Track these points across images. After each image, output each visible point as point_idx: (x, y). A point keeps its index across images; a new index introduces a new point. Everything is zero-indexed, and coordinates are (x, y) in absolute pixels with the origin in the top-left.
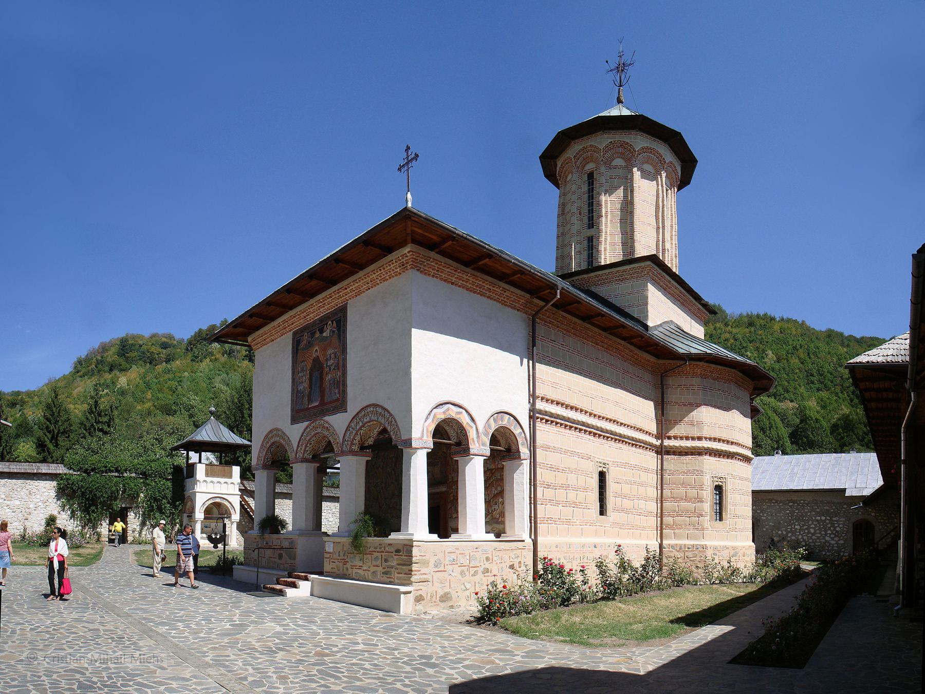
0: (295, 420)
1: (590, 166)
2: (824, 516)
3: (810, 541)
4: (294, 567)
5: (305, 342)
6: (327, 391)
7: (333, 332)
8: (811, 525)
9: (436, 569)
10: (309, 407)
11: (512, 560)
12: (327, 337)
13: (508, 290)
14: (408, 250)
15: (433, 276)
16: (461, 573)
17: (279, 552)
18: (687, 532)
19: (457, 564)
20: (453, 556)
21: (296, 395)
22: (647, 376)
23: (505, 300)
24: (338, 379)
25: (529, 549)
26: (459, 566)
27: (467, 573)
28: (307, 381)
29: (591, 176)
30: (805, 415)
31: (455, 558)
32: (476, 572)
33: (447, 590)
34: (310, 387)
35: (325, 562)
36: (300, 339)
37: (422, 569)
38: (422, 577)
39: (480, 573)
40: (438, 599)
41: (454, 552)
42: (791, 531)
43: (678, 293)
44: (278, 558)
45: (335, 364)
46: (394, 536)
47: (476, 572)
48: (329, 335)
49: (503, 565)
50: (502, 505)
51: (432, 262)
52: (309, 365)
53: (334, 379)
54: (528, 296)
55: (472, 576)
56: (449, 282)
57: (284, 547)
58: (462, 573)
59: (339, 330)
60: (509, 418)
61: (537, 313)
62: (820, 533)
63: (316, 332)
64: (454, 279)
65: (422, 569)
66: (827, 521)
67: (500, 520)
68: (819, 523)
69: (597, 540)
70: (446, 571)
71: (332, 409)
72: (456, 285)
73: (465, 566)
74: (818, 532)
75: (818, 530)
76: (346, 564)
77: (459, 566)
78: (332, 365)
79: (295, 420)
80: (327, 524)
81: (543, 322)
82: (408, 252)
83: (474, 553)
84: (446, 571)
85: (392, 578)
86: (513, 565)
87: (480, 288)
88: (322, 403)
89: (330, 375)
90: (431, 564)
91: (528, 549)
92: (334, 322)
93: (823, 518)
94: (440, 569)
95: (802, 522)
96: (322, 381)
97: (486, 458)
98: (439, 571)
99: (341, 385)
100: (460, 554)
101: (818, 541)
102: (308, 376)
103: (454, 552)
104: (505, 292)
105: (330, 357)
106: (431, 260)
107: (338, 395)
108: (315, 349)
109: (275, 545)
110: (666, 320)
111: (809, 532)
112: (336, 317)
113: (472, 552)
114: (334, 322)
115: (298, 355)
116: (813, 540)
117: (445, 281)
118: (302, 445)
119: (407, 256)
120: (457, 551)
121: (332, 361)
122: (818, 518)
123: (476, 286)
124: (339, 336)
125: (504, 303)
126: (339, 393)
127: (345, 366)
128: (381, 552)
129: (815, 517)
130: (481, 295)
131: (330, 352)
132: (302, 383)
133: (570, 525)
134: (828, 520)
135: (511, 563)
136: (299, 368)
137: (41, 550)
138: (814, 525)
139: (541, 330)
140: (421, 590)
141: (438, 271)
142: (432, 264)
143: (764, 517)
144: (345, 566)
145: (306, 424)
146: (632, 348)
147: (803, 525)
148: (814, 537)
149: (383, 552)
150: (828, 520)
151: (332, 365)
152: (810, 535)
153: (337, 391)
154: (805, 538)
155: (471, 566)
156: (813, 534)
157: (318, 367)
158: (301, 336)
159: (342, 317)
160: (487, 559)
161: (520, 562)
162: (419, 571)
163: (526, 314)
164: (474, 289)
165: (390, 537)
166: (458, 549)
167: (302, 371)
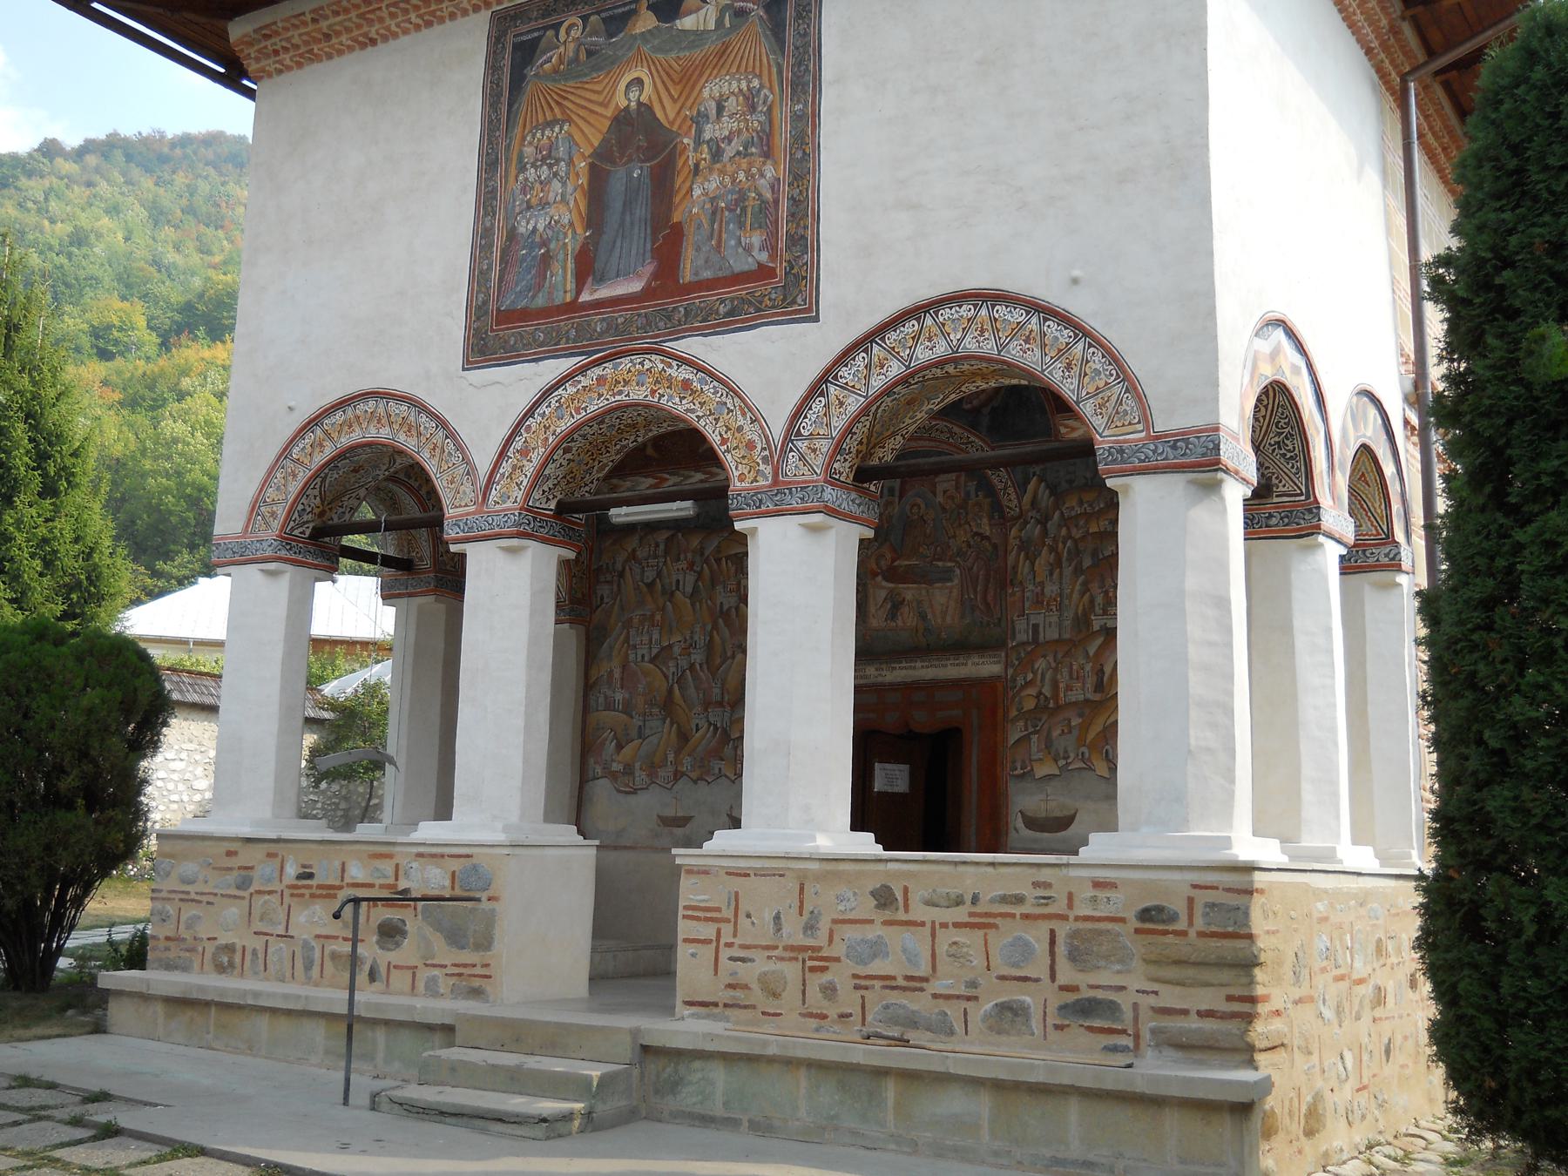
10: (585, 297)
24: (768, 195)
30: (104, 599)
36: (539, 39)
45: (745, 135)
46: (723, 841)
48: (712, 26)
53: (742, 196)
71: (722, 310)
76: (824, 969)
78: (729, 139)
80: (185, 798)
85: (1124, 1032)
88: (666, 279)
102: (583, 180)
105: (720, 109)
108: (636, 75)
115: (525, 98)
118: (524, 452)
121: (728, 125)
126: (770, 246)
136: (529, 150)
137: (1195, 1057)
145: (565, 365)
149: (1064, 918)
151: (729, 139)
153: (756, 239)
158: (546, 28)
167: (547, 157)
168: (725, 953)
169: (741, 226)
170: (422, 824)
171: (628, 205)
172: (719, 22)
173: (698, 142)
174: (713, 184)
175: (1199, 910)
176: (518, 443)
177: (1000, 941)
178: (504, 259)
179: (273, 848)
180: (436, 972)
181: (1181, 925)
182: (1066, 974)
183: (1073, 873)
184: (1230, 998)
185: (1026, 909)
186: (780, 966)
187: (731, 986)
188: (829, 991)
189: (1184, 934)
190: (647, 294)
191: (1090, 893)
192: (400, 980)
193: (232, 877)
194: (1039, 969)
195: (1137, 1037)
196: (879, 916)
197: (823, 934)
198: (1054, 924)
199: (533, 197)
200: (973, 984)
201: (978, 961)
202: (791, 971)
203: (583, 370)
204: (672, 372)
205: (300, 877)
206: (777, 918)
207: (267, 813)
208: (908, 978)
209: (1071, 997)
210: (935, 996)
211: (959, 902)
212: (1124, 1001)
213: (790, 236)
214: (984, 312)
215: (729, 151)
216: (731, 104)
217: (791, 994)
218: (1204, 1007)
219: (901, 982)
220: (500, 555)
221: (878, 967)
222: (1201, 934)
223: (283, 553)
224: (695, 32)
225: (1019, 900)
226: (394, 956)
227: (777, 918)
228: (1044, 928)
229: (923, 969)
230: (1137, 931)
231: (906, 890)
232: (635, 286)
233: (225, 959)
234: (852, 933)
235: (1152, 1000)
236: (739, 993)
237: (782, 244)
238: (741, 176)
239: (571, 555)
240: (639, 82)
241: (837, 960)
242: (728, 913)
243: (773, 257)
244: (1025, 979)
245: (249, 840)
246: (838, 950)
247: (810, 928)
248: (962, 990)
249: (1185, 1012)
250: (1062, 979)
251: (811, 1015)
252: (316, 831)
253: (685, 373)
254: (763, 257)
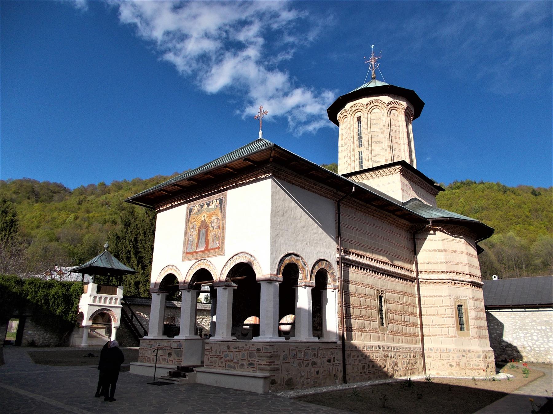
0: (184, 259)
1: (358, 114)
2: (543, 325)
3: (535, 346)
4: (180, 362)
5: (196, 210)
6: (211, 241)
7: (217, 206)
8: (533, 333)
9: (284, 361)
10: (197, 251)
11: (329, 356)
12: (212, 209)
13: (324, 188)
14: (269, 165)
15: (283, 180)
16: (299, 365)
17: (169, 351)
18: (441, 338)
19: (296, 358)
20: (294, 352)
21: (187, 242)
22: (404, 234)
23: (322, 193)
24: (219, 235)
25: (339, 348)
26: (298, 360)
27: (302, 365)
28: (197, 234)
29: (359, 119)
31: (296, 354)
32: (308, 364)
33: (290, 377)
34: (199, 239)
35: (205, 357)
37: (275, 361)
38: (276, 366)
39: (310, 364)
40: (285, 383)
41: (295, 350)
42: (516, 338)
43: (418, 181)
44: (167, 356)
47: (308, 364)
49: (324, 359)
50: (320, 318)
51: (282, 172)
52: (198, 224)
54: (335, 191)
55: (306, 366)
56: (291, 183)
57: (173, 348)
58: (300, 365)
59: (221, 205)
60: (326, 263)
61: (340, 200)
62: (543, 340)
63: (204, 205)
64: (294, 182)
65: (275, 361)
66: (548, 330)
67: (318, 328)
68: (541, 332)
69: (381, 343)
70: (289, 363)
72: (295, 184)
73: (301, 359)
74: (540, 339)
75: (540, 337)
76: (221, 359)
77: (298, 360)
79: (184, 259)
81: (343, 205)
82: (270, 166)
83: (306, 351)
84: (289, 363)
86: (330, 359)
87: (308, 186)
88: (207, 249)
89: (213, 232)
90: (281, 358)
91: (338, 348)
92: (218, 200)
93: (544, 328)
94: (286, 361)
95: (525, 330)
96: (207, 236)
97: (312, 288)
98: (287, 363)
99: (221, 238)
100: (299, 351)
101: (542, 346)
102: (197, 232)
103: (295, 350)
104: (322, 188)
105: (214, 221)
106: (282, 171)
107: (218, 245)
109: (165, 347)
110: (412, 198)
111: (532, 339)
112: (219, 198)
113: (306, 350)
114: (218, 200)
116: (537, 345)
117: (289, 182)
119: (269, 168)
120: (296, 349)
122: (539, 328)
123: (306, 185)
124: (221, 209)
125: (322, 195)
127: (224, 227)
128: (247, 350)
129: (536, 327)
130: (308, 190)
131: (214, 218)
132: (192, 235)
133: (363, 332)
134: (549, 329)
135: (329, 358)
136: (191, 226)
138: (537, 333)
139: (342, 210)
140: (274, 376)
141: (285, 177)
142: (283, 173)
143: (491, 326)
144: (221, 361)
146: (395, 217)
147: (527, 333)
148: (537, 343)
150: (549, 329)
152: (534, 341)
153: (218, 242)
154: (530, 344)
155: (305, 359)
156: (537, 341)
157: (204, 226)
159: (223, 198)
160: (315, 355)
161: (334, 358)
162: (274, 362)
163: (334, 200)
164: (305, 187)
165: (252, 340)
166: (297, 348)
167: (193, 227)
168: (210, 357)
169: (216, 240)
170: (175, 336)
171: (203, 236)
172: (214, 207)
173: (211, 226)
174: (213, 233)
175: (263, 348)
176: (188, 274)
177: (241, 354)
178: (187, 244)
179: (155, 341)
180: (175, 361)
181: (261, 351)
182: (249, 359)
183: (250, 343)
184: (267, 362)
185: (244, 349)
186: (216, 358)
187: (210, 362)
188: (222, 362)
189: (261, 352)
190: (205, 250)
191: (251, 346)
192: (171, 362)
193: (150, 346)
194: (245, 358)
195: (256, 369)
196: (228, 350)
197: (221, 353)
198: (247, 351)
199: (191, 233)
200: (238, 361)
201: (239, 357)
202: (217, 359)
203: (197, 262)
204: (207, 263)
205: (159, 346)
206: (216, 351)
207: (188, 335)
208: (231, 360)
209: (249, 362)
210: (234, 363)
211: (237, 348)
212: (255, 363)
213: (222, 242)
214: (238, 256)
215: (215, 228)
216: (216, 221)
217: (217, 363)
218: (264, 363)
219: (230, 361)
220: (187, 292)
221: (228, 358)
222: (264, 352)
223: (160, 291)
224: (211, 209)
225: (243, 347)
226: (170, 359)
227: (216, 351)
228: (246, 351)
229: (233, 359)
230: (257, 352)
231: (231, 346)
232: (203, 249)
233: (148, 360)
234: (225, 353)
235: (258, 363)
236: (211, 363)
237: (221, 243)
238: (216, 232)
239: (167, 294)
240: (204, 216)
241: (223, 357)
242: (210, 350)
243: (220, 245)
244: (244, 360)
245: (152, 340)
246: (223, 356)
247: (220, 352)
248: (237, 362)
249: (261, 364)
250: (248, 360)
251: (220, 366)
252: (166, 337)
253: (209, 263)
254: (218, 245)
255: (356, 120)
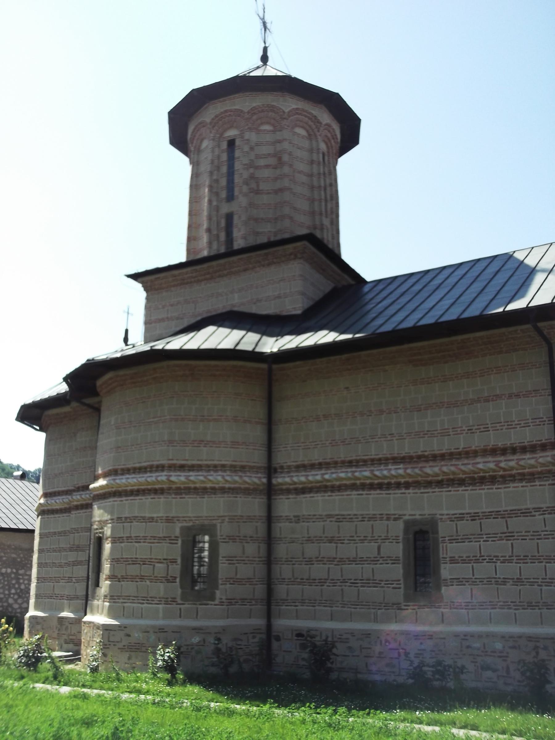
1: (232, 133)
29: (231, 143)
255: (224, 145)
